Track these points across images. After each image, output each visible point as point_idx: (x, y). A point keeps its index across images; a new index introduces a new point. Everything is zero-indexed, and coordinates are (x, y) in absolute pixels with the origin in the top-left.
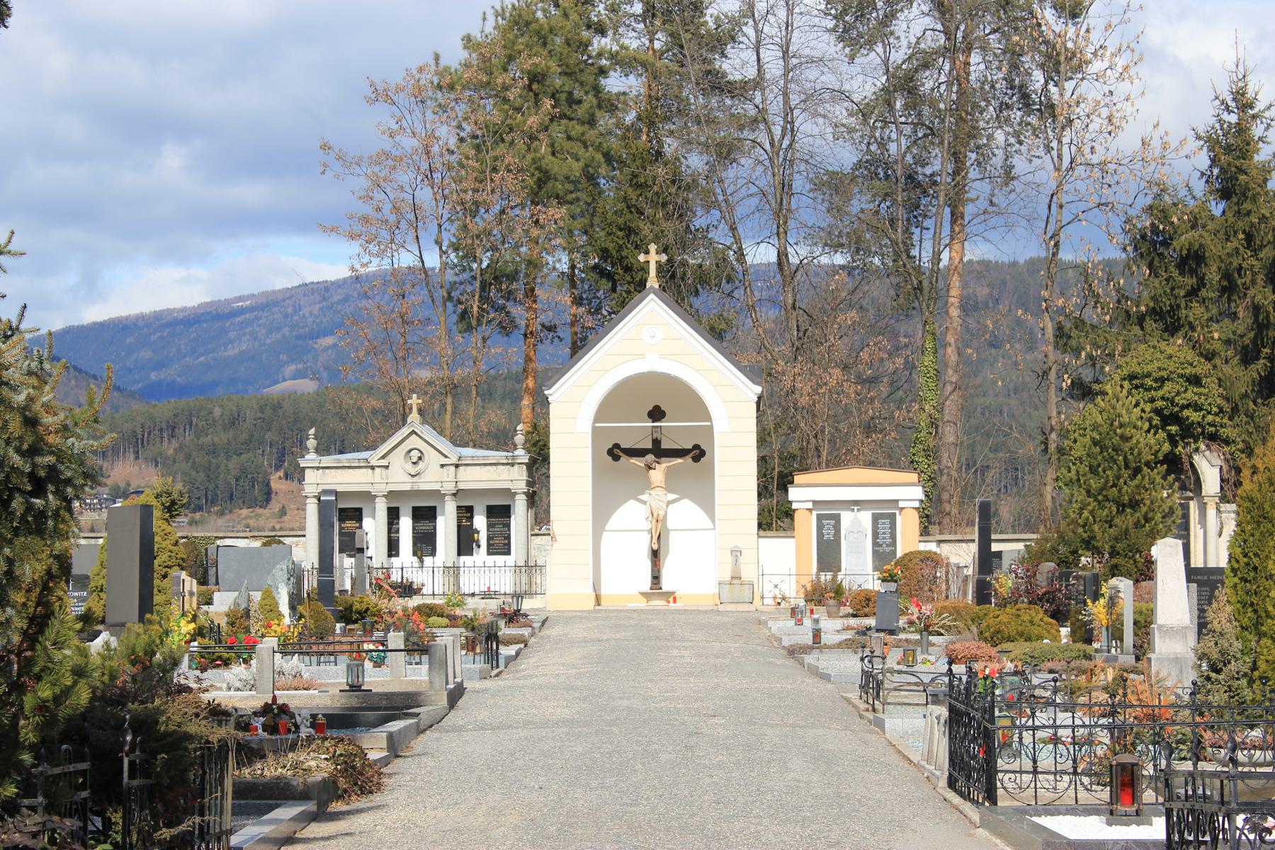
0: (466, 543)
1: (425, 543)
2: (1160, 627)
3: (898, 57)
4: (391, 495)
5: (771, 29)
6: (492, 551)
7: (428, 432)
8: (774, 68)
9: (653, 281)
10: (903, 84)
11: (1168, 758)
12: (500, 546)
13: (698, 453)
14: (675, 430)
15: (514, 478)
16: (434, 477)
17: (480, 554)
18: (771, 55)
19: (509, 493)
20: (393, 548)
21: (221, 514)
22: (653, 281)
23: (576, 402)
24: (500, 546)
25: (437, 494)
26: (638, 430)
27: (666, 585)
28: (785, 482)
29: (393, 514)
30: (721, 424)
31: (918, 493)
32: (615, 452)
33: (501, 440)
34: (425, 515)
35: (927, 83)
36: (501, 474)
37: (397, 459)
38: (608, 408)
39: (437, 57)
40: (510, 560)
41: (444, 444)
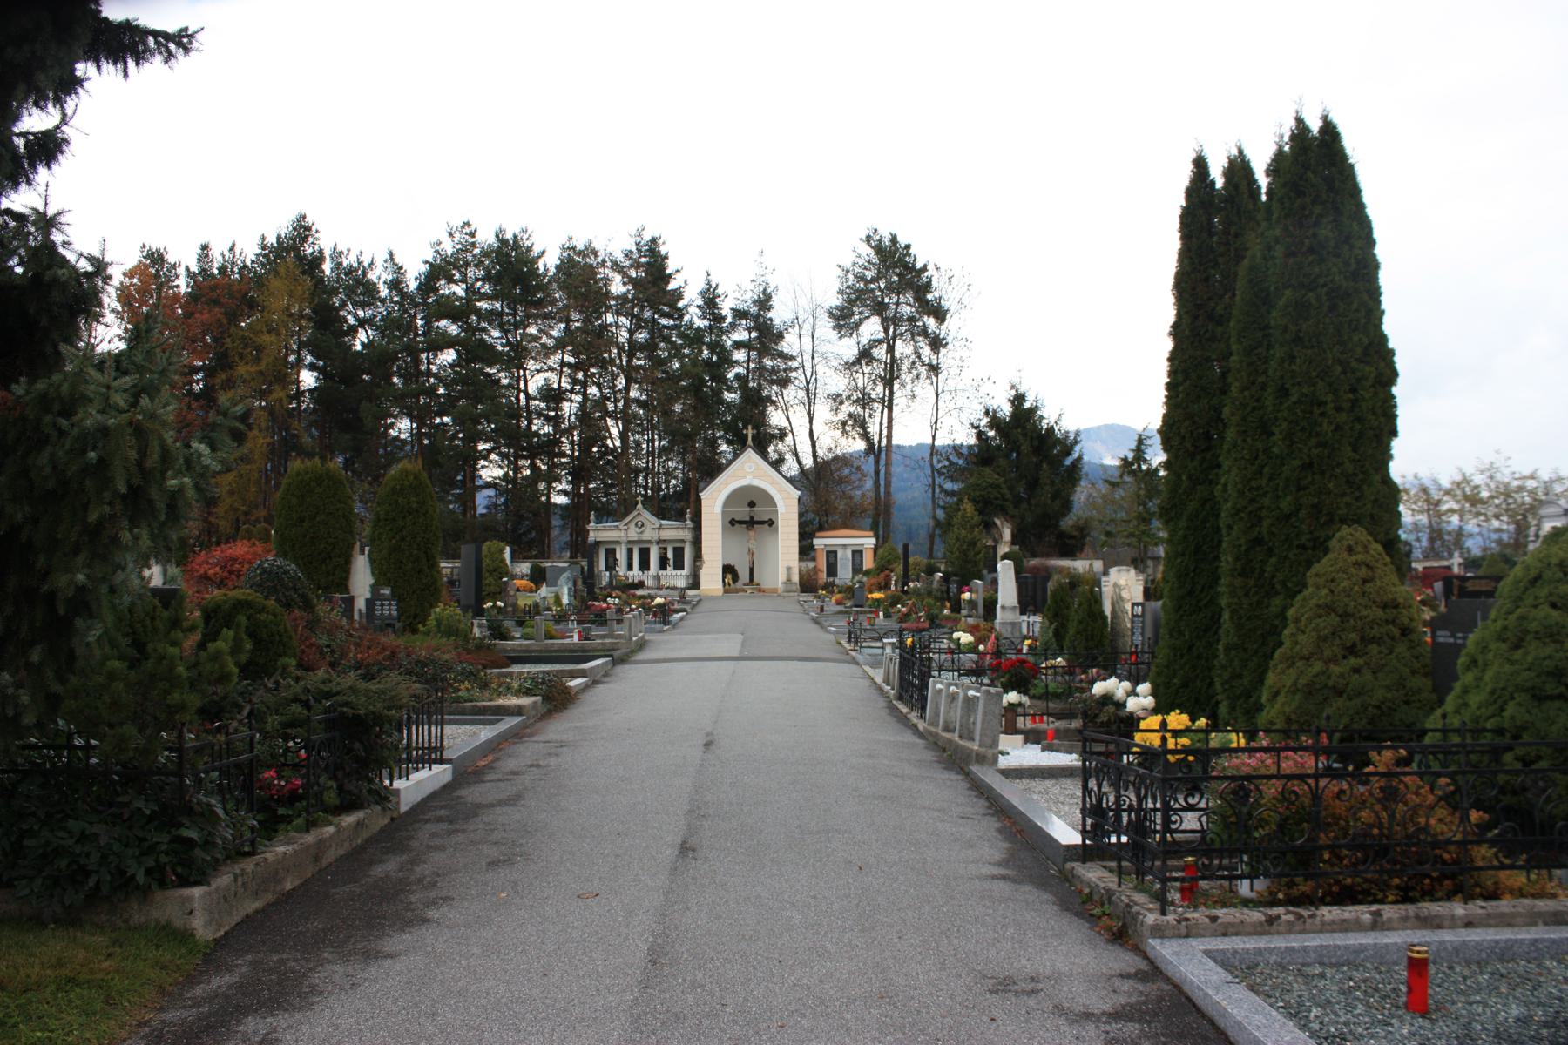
0: (663, 564)
1: (645, 565)
2: (1003, 607)
3: (864, 341)
4: (629, 542)
5: (807, 327)
6: (676, 568)
7: (646, 514)
8: (807, 347)
9: (750, 442)
10: (865, 355)
11: (1398, 887)
12: (679, 565)
13: (771, 523)
14: (761, 511)
15: (687, 535)
16: (649, 534)
17: (670, 570)
18: (807, 341)
19: (683, 541)
20: (630, 567)
21: (1000, 831)
22: (750, 442)
23: (714, 499)
24: (679, 565)
25: (650, 542)
26: (742, 511)
27: (756, 579)
28: (812, 536)
29: (630, 551)
30: (781, 508)
31: (873, 541)
32: (733, 522)
33: (680, 516)
34: (644, 554)
35: (876, 352)
36: (675, 531)
37: (632, 525)
38: (731, 500)
39: (126, 74)
40: (684, 572)
41: (653, 519)
